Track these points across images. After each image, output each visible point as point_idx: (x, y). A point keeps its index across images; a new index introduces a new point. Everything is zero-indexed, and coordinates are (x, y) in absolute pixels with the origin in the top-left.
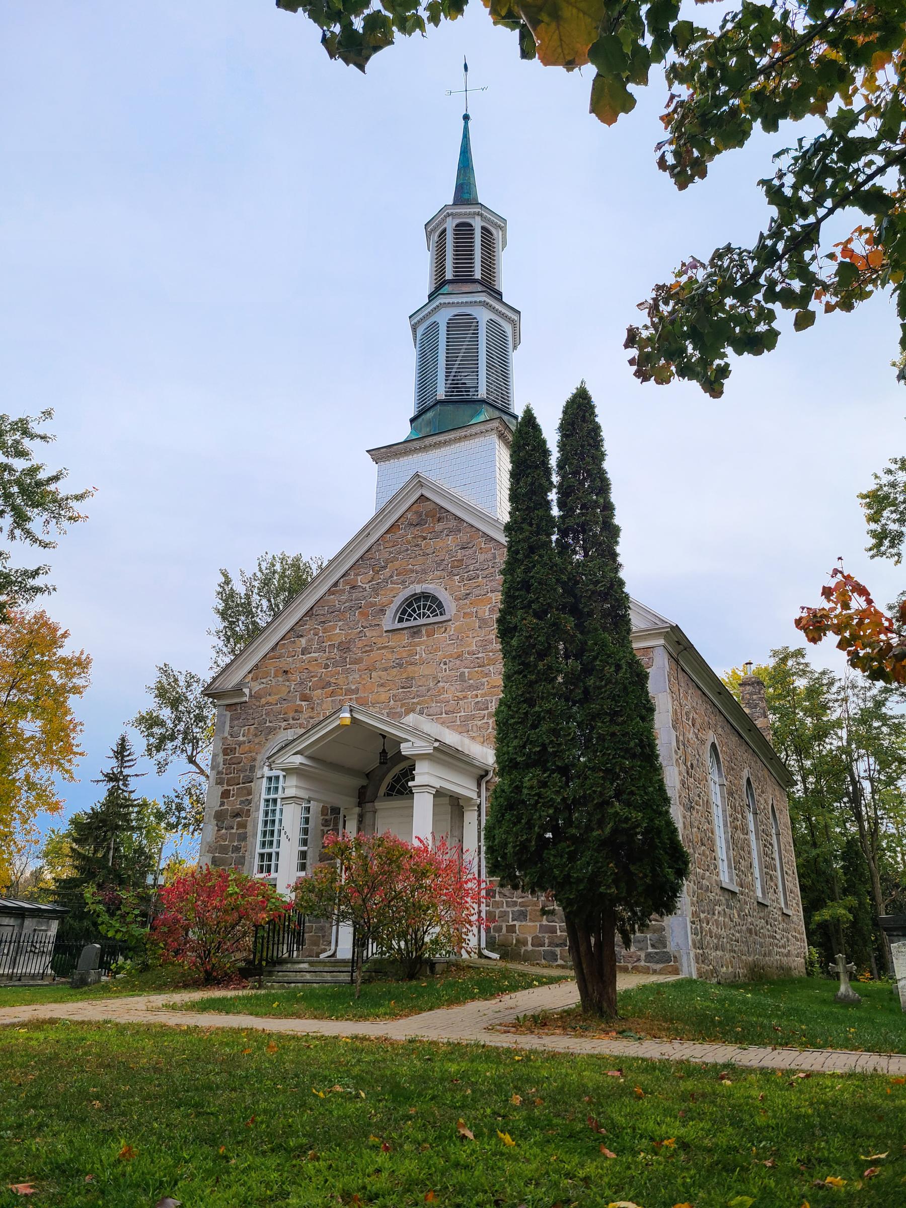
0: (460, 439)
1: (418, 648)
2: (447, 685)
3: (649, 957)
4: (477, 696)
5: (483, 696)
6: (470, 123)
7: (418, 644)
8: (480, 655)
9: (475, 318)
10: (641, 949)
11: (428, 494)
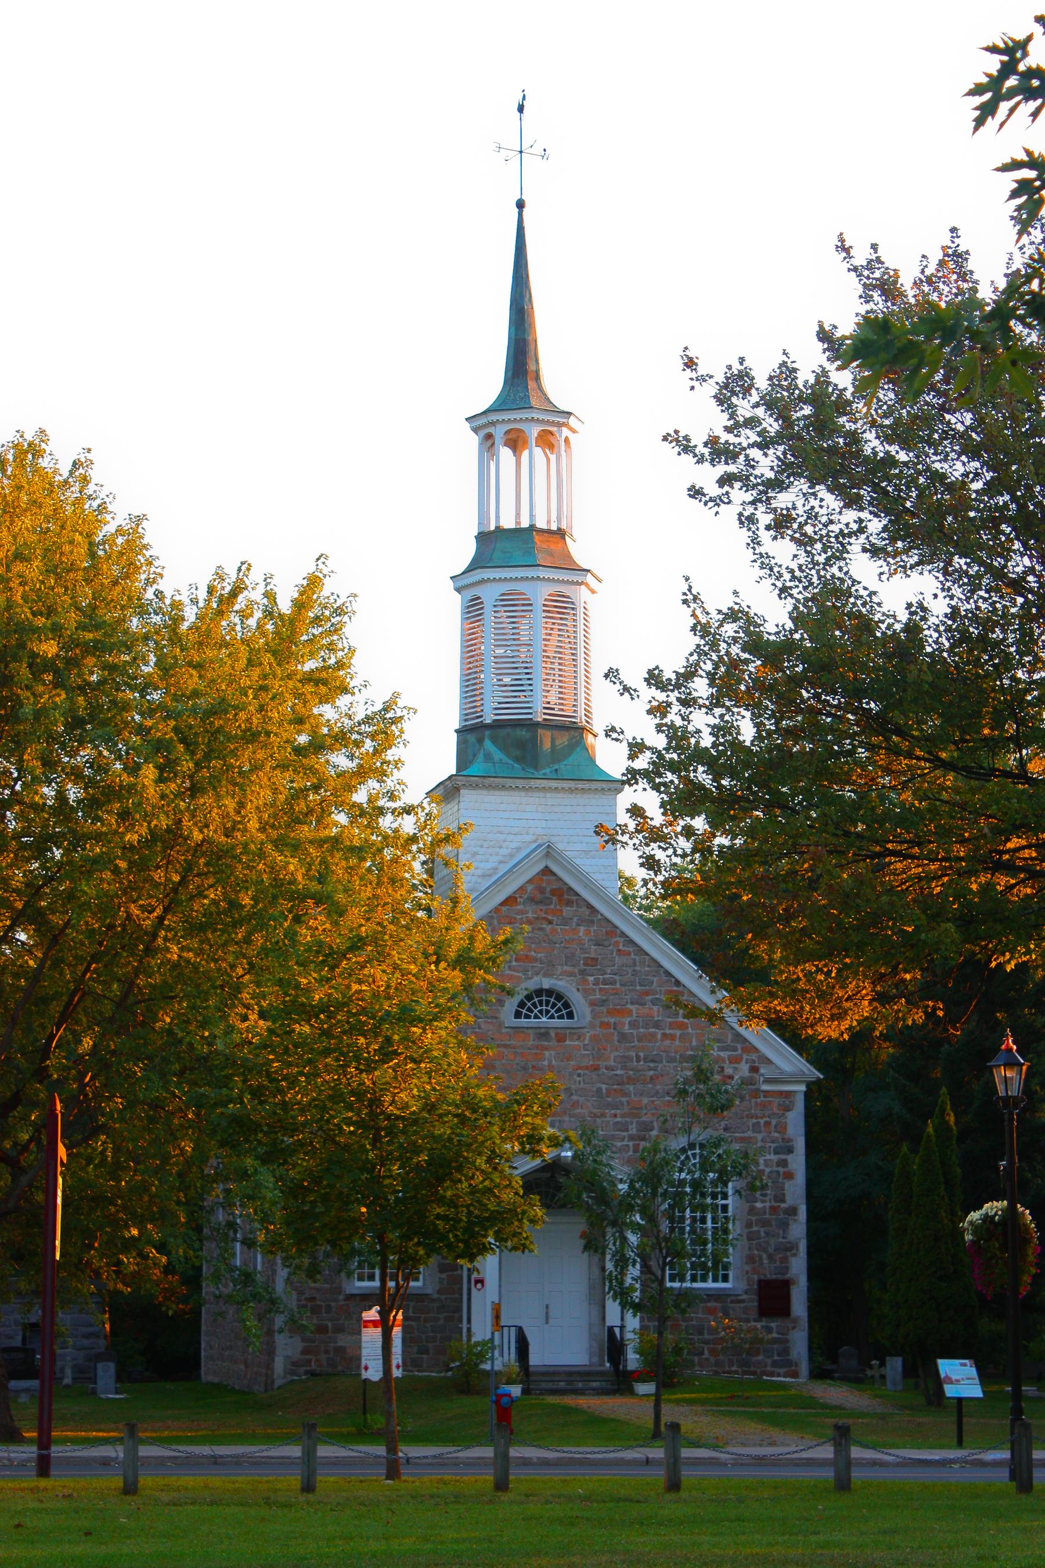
0: (571, 790)
1: (547, 1053)
2: (582, 1100)
3: (775, 1364)
4: (615, 1116)
5: (622, 1116)
6: (525, 210)
7: (547, 1049)
8: (618, 1072)
9: (573, 603)
10: (768, 1357)
11: (554, 868)
